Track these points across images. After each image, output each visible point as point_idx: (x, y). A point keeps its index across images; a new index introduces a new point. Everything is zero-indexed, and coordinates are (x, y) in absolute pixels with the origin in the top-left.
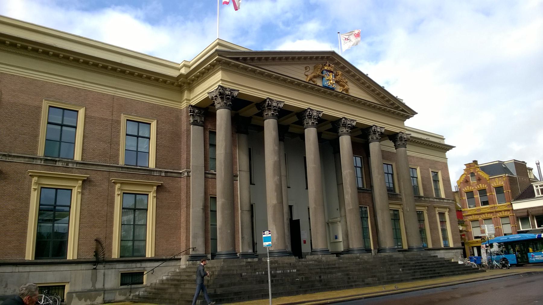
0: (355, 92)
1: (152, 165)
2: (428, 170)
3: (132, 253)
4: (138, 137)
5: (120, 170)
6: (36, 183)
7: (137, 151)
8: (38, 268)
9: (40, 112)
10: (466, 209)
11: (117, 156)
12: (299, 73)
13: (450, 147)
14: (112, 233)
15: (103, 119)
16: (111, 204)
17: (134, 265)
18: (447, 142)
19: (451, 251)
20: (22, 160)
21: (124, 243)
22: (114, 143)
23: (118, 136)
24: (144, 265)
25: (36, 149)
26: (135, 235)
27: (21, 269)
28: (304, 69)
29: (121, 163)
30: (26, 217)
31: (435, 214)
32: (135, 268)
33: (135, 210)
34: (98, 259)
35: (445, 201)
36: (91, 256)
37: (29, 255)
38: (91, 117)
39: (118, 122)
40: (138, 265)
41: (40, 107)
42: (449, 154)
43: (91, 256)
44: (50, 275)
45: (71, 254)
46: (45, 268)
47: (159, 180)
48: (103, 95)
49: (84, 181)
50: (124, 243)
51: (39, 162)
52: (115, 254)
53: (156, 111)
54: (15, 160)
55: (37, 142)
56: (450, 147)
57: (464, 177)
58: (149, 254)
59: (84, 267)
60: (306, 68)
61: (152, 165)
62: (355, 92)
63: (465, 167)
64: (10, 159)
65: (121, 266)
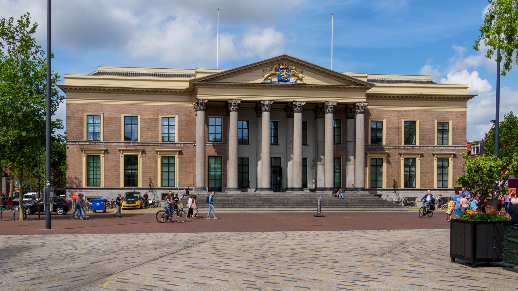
0: (309, 80)
1: (176, 141)
2: (433, 121)
4: (168, 179)
5: (159, 145)
6: (122, 154)
7: (215, 125)
11: (158, 137)
16: (156, 162)
17: (166, 191)
20: (115, 144)
22: (155, 131)
23: (158, 127)
30: (119, 169)
33: (168, 179)
38: (144, 119)
39: (157, 119)
41: (120, 118)
44: (410, 194)
47: (180, 148)
48: (149, 106)
51: (122, 144)
52: (159, 186)
53: (178, 110)
54: (113, 144)
60: (263, 71)
61: (176, 141)
62: (309, 80)
64: (110, 144)
65: (162, 191)
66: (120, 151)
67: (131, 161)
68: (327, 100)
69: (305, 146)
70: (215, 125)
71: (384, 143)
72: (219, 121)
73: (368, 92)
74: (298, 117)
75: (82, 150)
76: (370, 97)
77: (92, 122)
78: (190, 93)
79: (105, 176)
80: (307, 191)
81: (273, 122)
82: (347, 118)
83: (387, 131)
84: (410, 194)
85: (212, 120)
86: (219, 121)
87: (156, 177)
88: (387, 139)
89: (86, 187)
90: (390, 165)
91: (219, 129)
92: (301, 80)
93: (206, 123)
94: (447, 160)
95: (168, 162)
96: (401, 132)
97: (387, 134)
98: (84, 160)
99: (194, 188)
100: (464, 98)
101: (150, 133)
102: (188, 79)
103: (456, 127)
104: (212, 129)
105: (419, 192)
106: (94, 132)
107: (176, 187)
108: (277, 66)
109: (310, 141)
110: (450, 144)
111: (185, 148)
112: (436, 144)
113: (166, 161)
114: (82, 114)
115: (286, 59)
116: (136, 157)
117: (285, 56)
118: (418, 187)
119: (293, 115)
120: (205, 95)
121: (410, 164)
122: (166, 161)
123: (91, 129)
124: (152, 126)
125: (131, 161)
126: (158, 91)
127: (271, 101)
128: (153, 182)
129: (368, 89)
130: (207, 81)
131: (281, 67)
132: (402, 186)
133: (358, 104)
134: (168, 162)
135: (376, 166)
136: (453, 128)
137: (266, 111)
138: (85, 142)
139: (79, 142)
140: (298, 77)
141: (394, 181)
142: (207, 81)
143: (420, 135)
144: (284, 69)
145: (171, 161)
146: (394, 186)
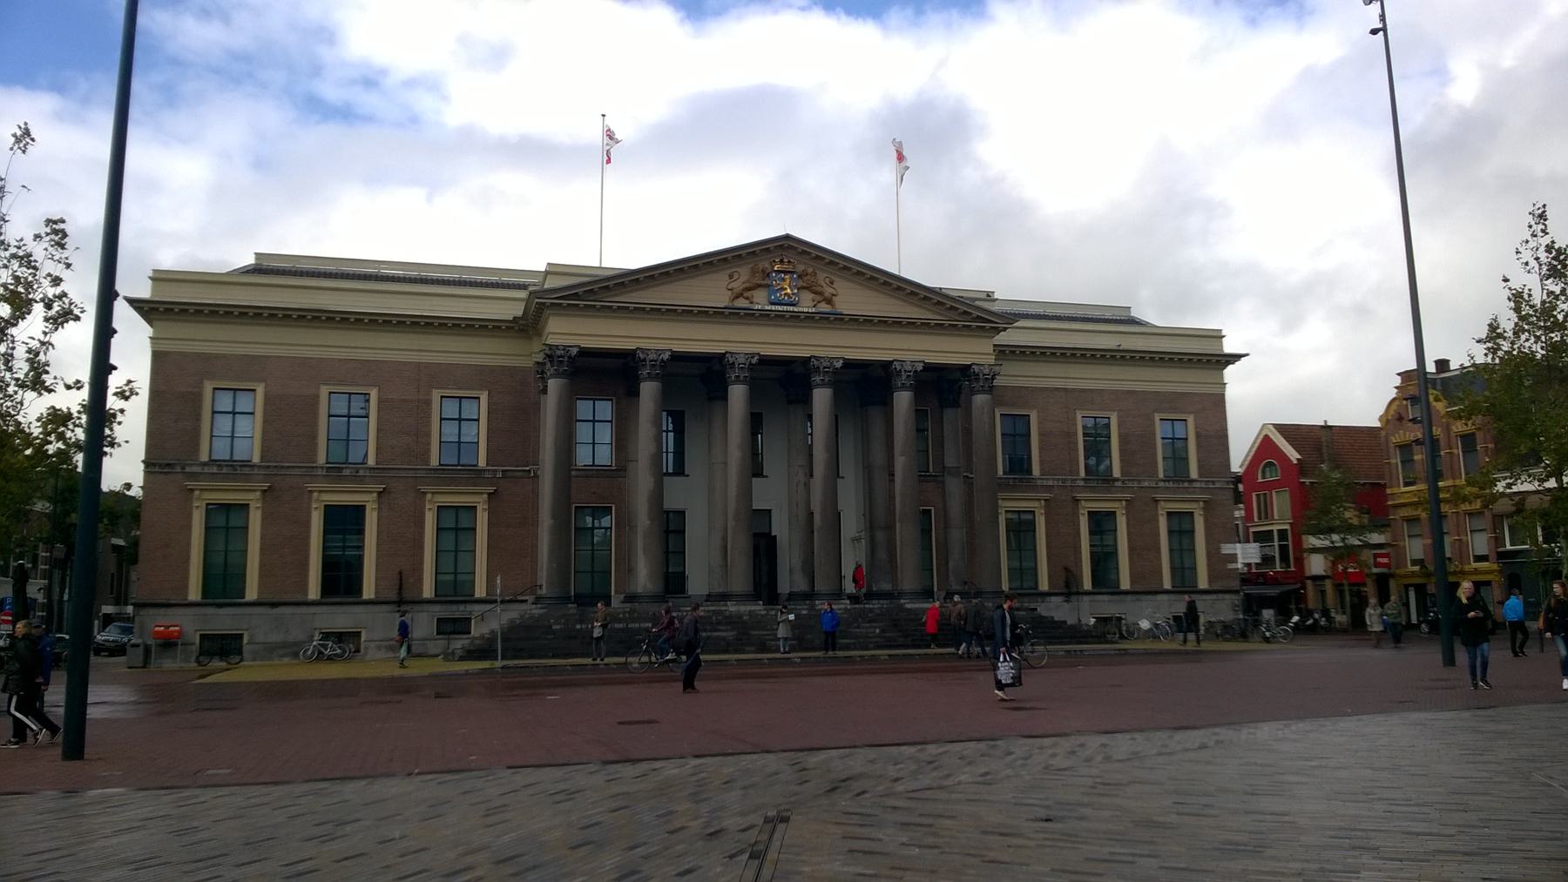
0: (852, 300)
3: (454, 589)
8: (325, 608)
9: (317, 403)
10: (1395, 490)
11: (427, 452)
12: (713, 292)
13: (1236, 358)
14: (421, 562)
15: (405, 401)
17: (454, 607)
18: (1229, 347)
19: (426, 607)
20: (297, 472)
21: (441, 577)
22: (422, 434)
23: (428, 424)
24: (469, 607)
25: (186, 587)
26: (152, 611)
27: (303, 610)
29: (434, 462)
30: (421, 547)
31: (1076, 515)
32: (457, 611)
34: (402, 598)
35: (1198, 485)
36: (393, 596)
37: (314, 592)
39: (428, 403)
40: (462, 607)
42: (1230, 372)
43: (393, 596)
44: (340, 618)
45: (368, 592)
46: (333, 608)
49: (380, 493)
50: (441, 577)
52: (428, 592)
55: (316, 444)
56: (1236, 358)
57: (1394, 407)
58: (480, 591)
59: (384, 607)
60: (731, 276)
61: (482, 463)
62: (852, 300)
63: (1398, 381)
65: (437, 608)
67: (344, 521)
68: (817, 354)
70: (460, 420)
71: (1036, 471)
73: (1003, 338)
74: (903, 400)
76: (1003, 352)
77: (345, 412)
78: (526, 327)
79: (262, 566)
81: (670, 413)
83: (1041, 442)
84: (223, 621)
85: (584, 408)
86: (605, 409)
88: (1042, 462)
91: (605, 434)
92: (829, 301)
94: (245, 507)
96: (1076, 444)
97: (1041, 449)
99: (531, 598)
102: (523, 294)
105: (1129, 598)
107: (477, 595)
108: (767, 265)
110: (1194, 474)
112: (1161, 476)
113: (220, 520)
114: (200, 385)
115: (790, 247)
116: (359, 510)
117: (787, 237)
118: (1125, 585)
119: (726, 391)
120: (567, 332)
122: (449, 522)
123: (450, 431)
125: (344, 521)
126: (418, 323)
127: (753, 355)
129: (997, 331)
130: (576, 296)
132: (1087, 585)
133: (976, 368)
135: (457, 529)
136: (1198, 436)
137: (738, 381)
138: (204, 464)
140: (821, 293)
141: (1067, 569)
142: (576, 296)
143: (1122, 452)
144: (785, 272)
145: (235, 521)
146: (1067, 585)
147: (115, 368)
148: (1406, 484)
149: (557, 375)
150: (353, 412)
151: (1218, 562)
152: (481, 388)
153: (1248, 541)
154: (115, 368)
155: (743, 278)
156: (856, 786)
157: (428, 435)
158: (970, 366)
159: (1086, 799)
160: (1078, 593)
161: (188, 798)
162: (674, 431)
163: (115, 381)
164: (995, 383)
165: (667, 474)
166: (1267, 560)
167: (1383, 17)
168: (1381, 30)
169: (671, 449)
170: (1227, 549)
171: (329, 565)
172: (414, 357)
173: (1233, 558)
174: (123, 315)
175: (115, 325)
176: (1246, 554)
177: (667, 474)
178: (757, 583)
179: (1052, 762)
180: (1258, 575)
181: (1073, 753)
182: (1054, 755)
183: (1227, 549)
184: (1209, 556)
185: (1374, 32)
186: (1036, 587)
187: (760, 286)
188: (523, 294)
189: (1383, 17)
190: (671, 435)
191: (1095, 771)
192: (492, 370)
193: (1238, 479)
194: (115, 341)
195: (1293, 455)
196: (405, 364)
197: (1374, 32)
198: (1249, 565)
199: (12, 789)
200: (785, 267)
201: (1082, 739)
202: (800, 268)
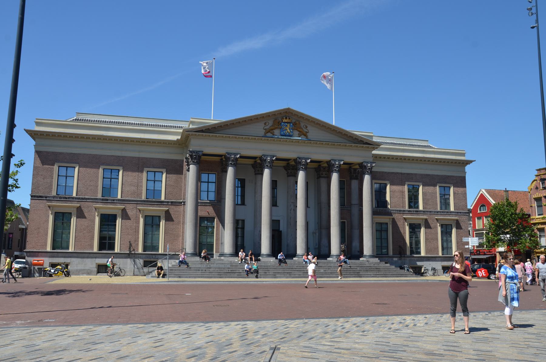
7: (208, 182)
13: (468, 162)
14: (138, 238)
16: (138, 223)
23: (142, 182)
28: (264, 125)
37: (95, 249)
42: (468, 168)
56: (468, 162)
60: (265, 124)
66: (96, 209)
69: (274, 208)
70: (208, 182)
72: (213, 177)
75: (49, 207)
77: (109, 176)
80: (236, 260)
81: (239, 179)
82: (351, 178)
85: (204, 177)
86: (213, 177)
87: (137, 240)
89: (52, 251)
90: (429, 230)
91: (212, 187)
93: (199, 179)
95: (152, 223)
98: (51, 218)
100: (463, 163)
101: (133, 188)
103: (457, 192)
104: (204, 186)
106: (154, 190)
109: (281, 201)
111: (172, 207)
117: (289, 109)
121: (108, 221)
122: (384, 226)
124: (136, 181)
128: (133, 245)
131: (284, 120)
134: (152, 223)
139: (46, 198)
141: (400, 247)
147: (14, 156)
148: (539, 215)
149: (194, 163)
150: (113, 177)
151: (461, 244)
152: (163, 168)
153: (473, 237)
154: (14, 156)
155: (270, 125)
156: (309, 335)
157: (142, 186)
158: (330, 161)
159: (405, 343)
160: (404, 257)
161: (34, 331)
162: (241, 187)
163: (13, 161)
164: (373, 170)
165: (237, 204)
166: (481, 245)
167: (537, 21)
168: (536, 27)
169: (239, 194)
170: (465, 240)
171: (102, 239)
172: (137, 155)
173: (467, 243)
174: (18, 133)
175: (14, 138)
176: (473, 242)
177: (237, 204)
178: (272, 253)
179: (392, 326)
180: (477, 250)
181: (400, 323)
182: (393, 324)
183: (465, 240)
184: (457, 243)
185: (533, 28)
186: (388, 254)
187: (276, 128)
188: (181, 131)
189: (537, 21)
190: (240, 189)
191: (409, 331)
192: (168, 160)
193: (470, 211)
194: (14, 145)
195: (493, 202)
196: (133, 158)
197: (533, 28)
198: (474, 246)
199: (67, 308)
200: (289, 121)
201: (404, 317)
202: (294, 121)
